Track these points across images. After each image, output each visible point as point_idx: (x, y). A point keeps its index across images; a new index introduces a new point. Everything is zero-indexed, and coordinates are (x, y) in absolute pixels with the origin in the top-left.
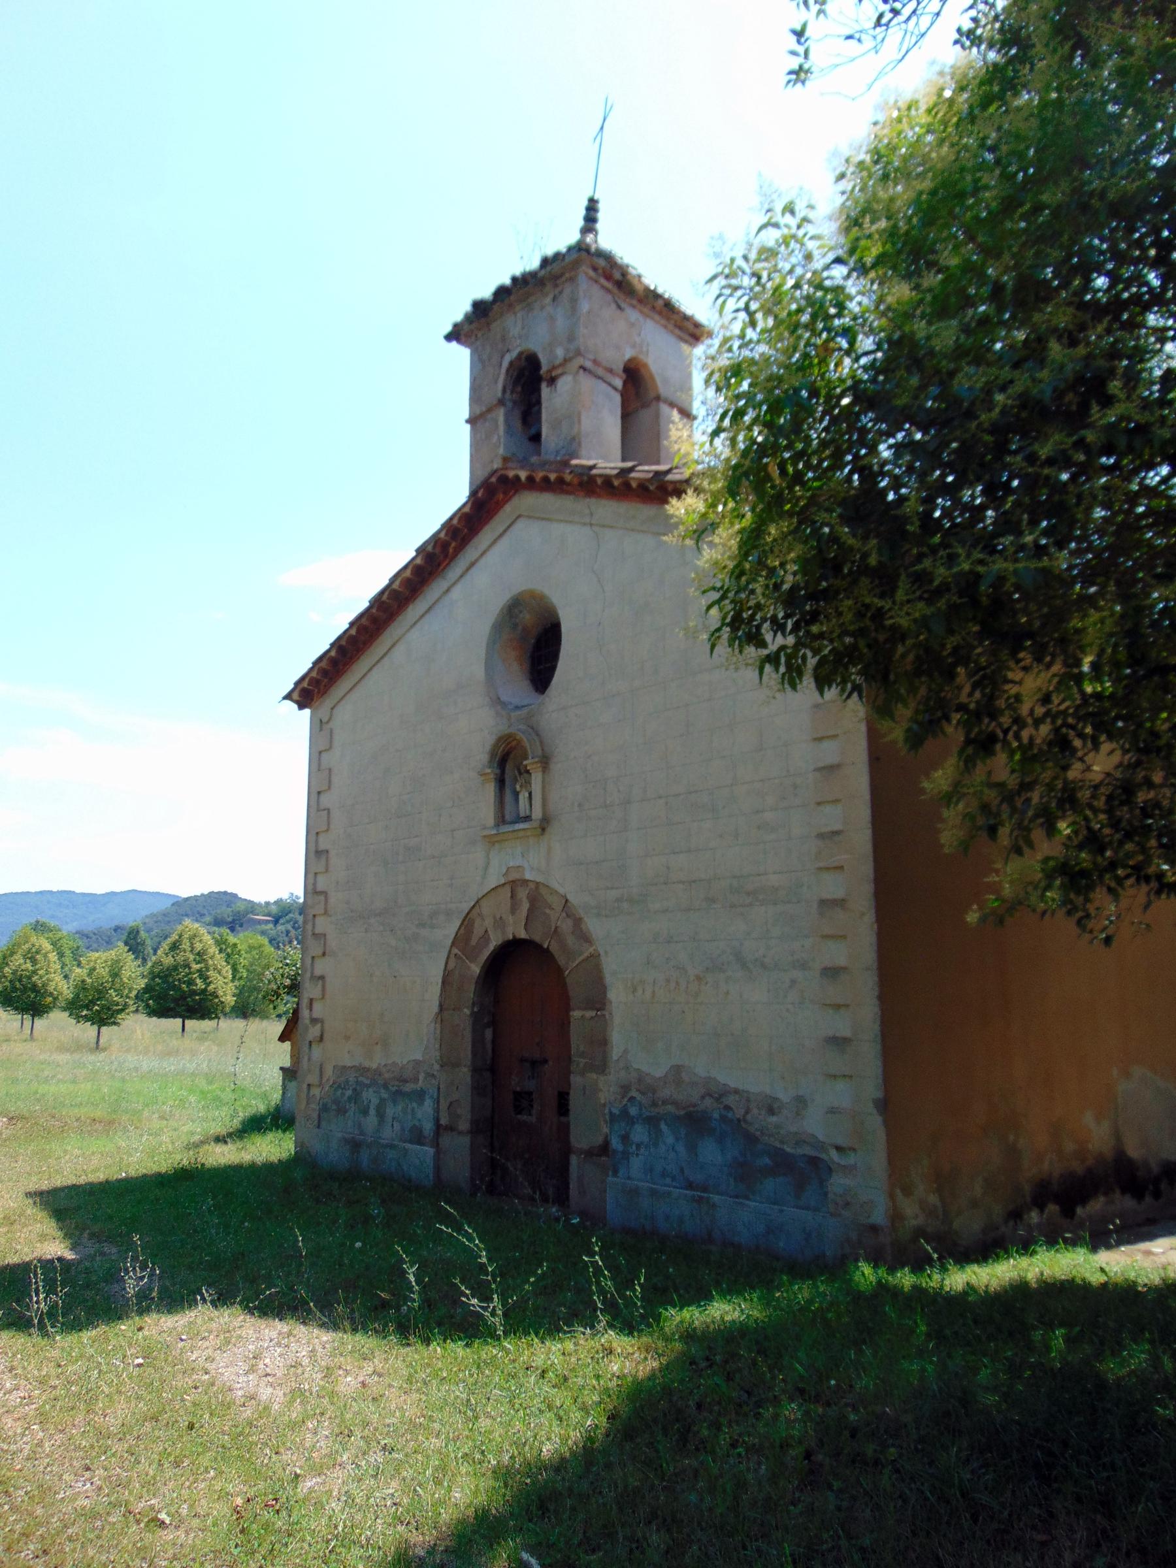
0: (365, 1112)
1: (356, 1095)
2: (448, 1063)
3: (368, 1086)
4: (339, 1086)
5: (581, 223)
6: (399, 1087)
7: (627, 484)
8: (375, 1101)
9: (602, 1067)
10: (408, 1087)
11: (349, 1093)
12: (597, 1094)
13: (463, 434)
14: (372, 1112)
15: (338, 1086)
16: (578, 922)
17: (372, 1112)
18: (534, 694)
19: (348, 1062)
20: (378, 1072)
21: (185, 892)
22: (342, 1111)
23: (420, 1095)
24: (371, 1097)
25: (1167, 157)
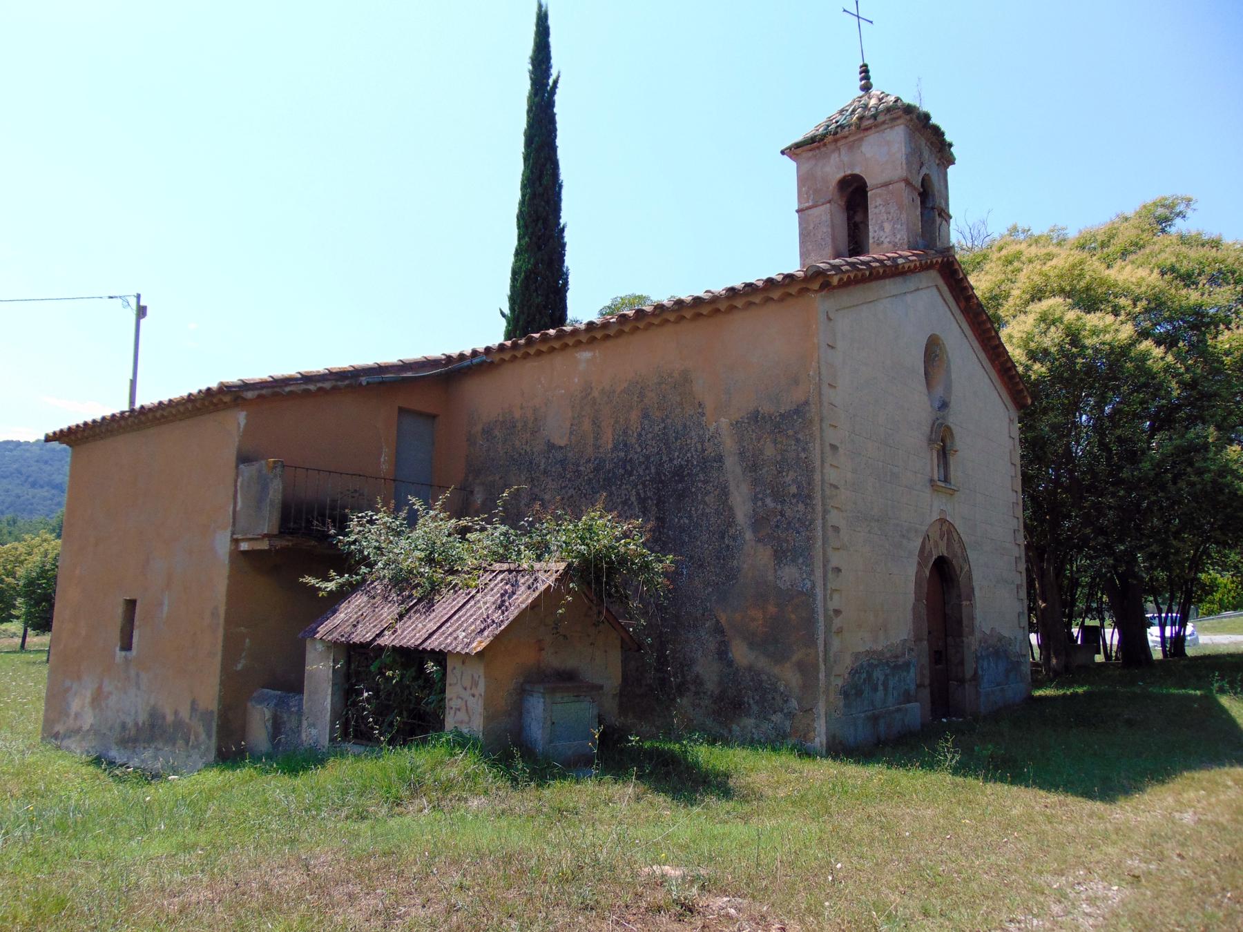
0: (875, 689)
1: (870, 675)
2: (918, 639)
3: (876, 666)
4: (856, 672)
5: (859, 83)
6: (895, 665)
7: (984, 322)
8: (882, 678)
9: (972, 632)
10: (901, 661)
11: (864, 676)
12: (973, 643)
13: (512, 259)
14: (881, 687)
15: (854, 672)
16: (964, 548)
17: (881, 687)
18: (942, 336)
19: (862, 649)
20: (882, 653)
21: (558, 98)
22: (859, 693)
23: (907, 665)
24: (878, 674)
25: (1157, 654)
